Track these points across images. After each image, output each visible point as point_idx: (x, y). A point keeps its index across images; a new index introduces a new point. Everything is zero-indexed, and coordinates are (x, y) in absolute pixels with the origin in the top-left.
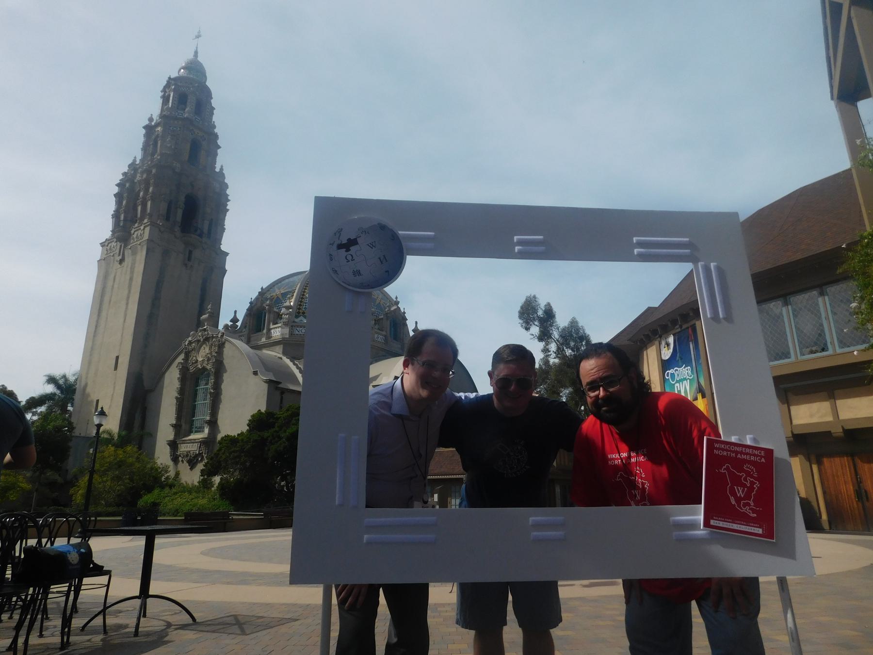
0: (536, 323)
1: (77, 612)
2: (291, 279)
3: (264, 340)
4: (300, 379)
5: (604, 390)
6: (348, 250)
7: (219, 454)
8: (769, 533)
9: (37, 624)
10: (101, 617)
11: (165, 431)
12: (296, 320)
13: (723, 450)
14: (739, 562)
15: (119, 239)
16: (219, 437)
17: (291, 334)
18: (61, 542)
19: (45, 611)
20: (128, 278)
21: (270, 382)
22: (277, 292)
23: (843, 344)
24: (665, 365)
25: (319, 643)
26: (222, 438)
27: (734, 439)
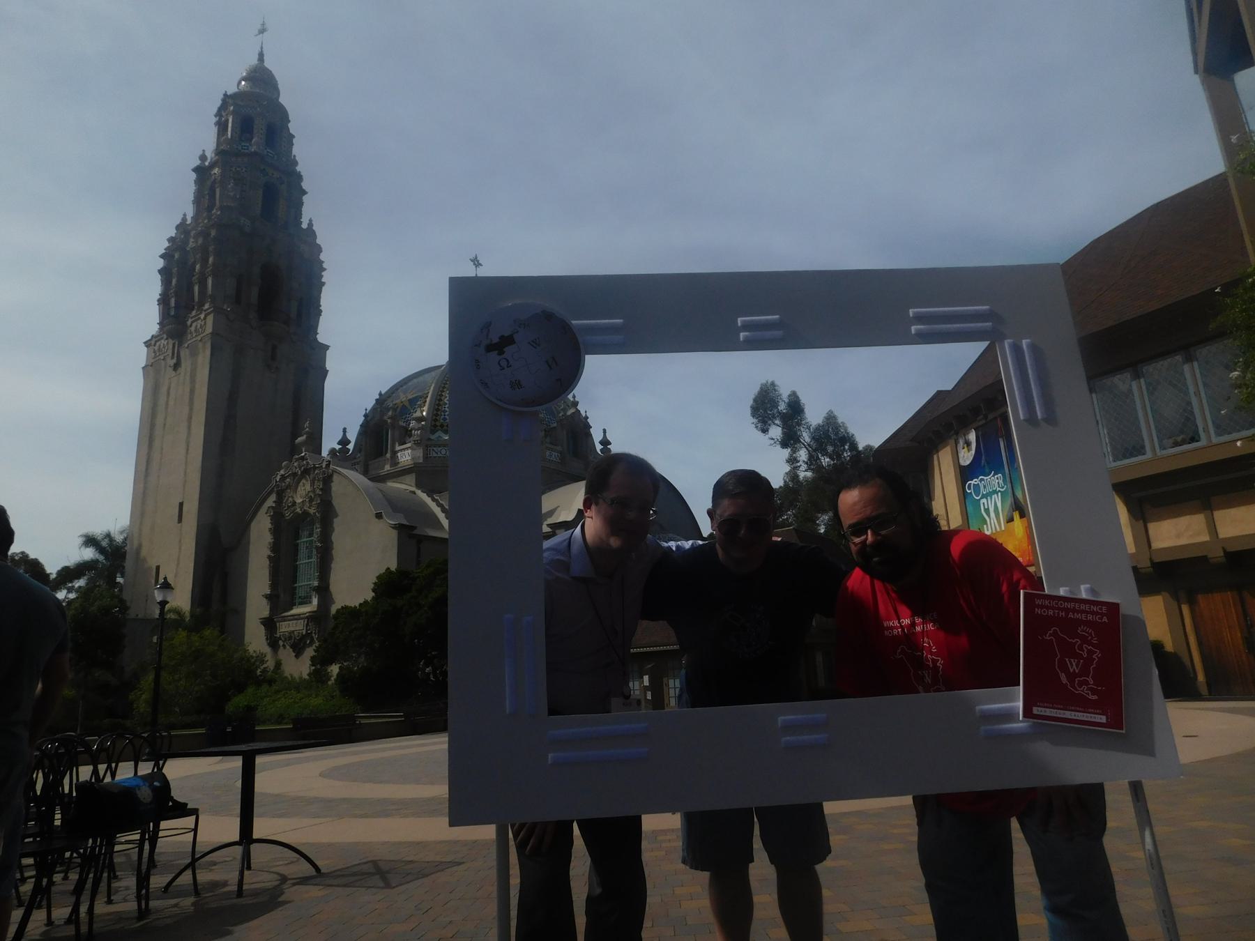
0: (777, 422)
1: (155, 866)
2: (421, 379)
3: (387, 467)
4: (445, 523)
5: (874, 533)
6: (501, 353)
7: (335, 633)
8: (1116, 721)
9: (103, 886)
10: (189, 873)
11: (256, 605)
12: (433, 437)
13: (1048, 608)
14: (1075, 764)
15: (171, 335)
16: (333, 610)
17: (426, 457)
18: (125, 772)
19: (112, 868)
20: (187, 390)
21: (400, 528)
22: (403, 397)
23: (1220, 430)
24: (965, 474)
25: (495, 894)
26: (338, 611)
27: (1062, 592)
